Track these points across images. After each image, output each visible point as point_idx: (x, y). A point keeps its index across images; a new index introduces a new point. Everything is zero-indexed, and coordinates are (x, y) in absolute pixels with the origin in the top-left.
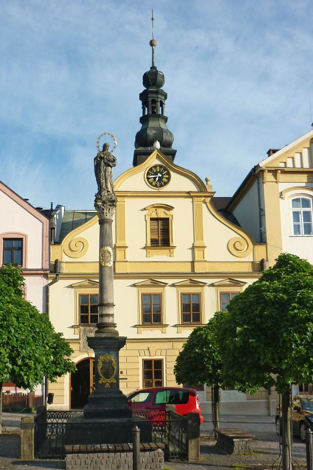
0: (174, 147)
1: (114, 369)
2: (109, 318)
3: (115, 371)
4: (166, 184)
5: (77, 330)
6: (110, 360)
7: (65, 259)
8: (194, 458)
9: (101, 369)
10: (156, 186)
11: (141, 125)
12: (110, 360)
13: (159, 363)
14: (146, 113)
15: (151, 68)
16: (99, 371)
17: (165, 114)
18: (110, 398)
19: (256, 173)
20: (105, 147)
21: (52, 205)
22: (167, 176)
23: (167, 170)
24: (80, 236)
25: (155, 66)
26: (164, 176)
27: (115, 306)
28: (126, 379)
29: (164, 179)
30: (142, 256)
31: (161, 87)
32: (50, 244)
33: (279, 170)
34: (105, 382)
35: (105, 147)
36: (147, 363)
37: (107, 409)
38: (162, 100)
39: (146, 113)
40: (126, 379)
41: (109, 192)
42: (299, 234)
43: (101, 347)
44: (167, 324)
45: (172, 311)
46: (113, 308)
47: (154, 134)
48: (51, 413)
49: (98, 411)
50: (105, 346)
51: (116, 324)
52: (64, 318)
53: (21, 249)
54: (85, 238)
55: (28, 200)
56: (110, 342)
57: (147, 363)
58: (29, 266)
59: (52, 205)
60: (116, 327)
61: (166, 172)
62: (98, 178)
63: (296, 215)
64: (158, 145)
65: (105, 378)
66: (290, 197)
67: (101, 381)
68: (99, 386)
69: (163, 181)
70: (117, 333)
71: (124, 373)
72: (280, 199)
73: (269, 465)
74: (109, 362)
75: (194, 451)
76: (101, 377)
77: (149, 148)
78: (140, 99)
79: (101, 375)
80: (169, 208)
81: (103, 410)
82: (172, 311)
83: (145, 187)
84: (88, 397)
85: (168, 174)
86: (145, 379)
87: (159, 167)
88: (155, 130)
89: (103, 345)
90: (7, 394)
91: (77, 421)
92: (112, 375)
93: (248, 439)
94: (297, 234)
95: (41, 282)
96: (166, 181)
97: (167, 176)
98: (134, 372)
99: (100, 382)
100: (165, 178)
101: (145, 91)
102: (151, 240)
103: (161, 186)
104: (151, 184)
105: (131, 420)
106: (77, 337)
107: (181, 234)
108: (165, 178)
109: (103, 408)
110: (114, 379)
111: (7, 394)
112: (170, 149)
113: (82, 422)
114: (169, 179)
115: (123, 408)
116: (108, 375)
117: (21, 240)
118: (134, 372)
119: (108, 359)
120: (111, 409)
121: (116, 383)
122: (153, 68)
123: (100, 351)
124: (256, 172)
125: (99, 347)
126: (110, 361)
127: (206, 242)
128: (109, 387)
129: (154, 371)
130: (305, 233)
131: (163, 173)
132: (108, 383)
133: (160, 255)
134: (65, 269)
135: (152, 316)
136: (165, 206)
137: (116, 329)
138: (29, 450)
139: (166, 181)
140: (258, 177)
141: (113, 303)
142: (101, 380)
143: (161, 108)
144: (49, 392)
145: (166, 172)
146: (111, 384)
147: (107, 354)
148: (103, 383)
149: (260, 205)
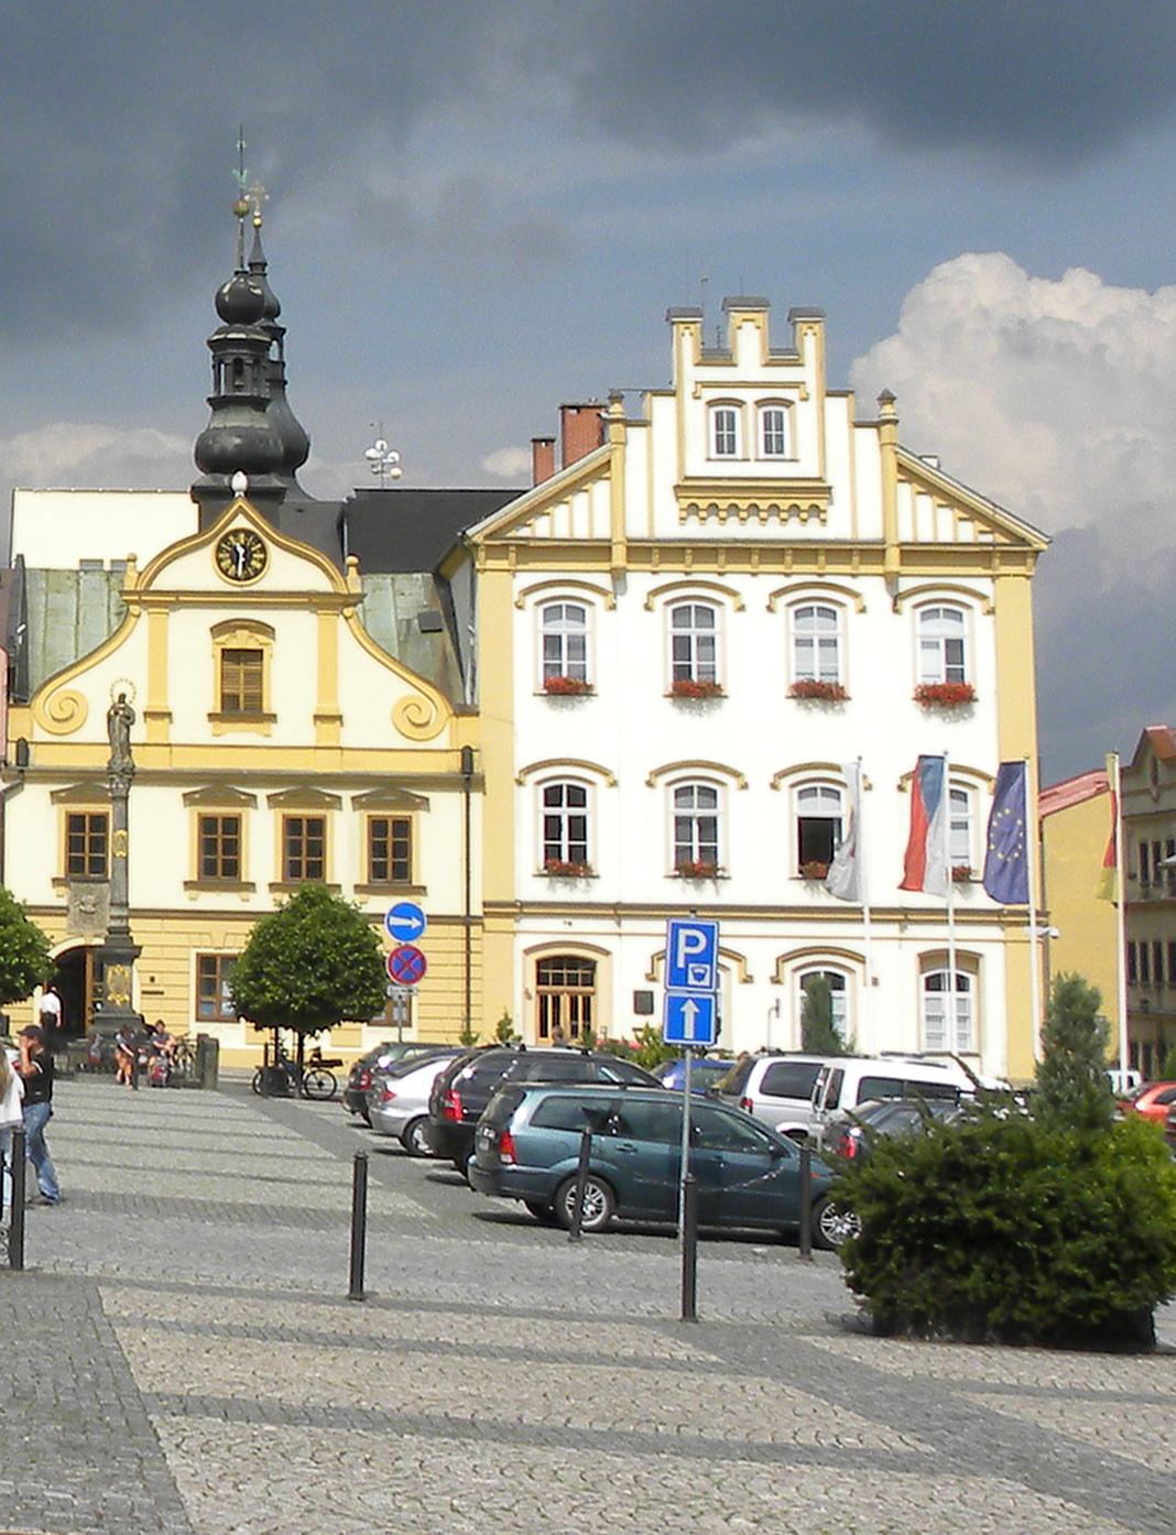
4: (257, 572)
5: (62, 890)
7: (40, 736)
10: (236, 578)
20: (122, 697)
22: (262, 556)
23: (260, 541)
24: (71, 686)
28: (162, 993)
29: (253, 563)
30: (204, 732)
32: (9, 706)
35: (122, 697)
40: (162, 993)
47: (237, 446)
48: (694, 912)
73: (1075, 1490)
80: (268, 630)
83: (212, 580)
84: (475, 1073)
85: (263, 550)
88: (239, 436)
96: (259, 566)
97: (262, 556)
98: (178, 979)
103: (248, 578)
104: (225, 572)
106: (63, 902)
114: (263, 562)
118: (178, 979)
134: (39, 758)
139: (259, 566)
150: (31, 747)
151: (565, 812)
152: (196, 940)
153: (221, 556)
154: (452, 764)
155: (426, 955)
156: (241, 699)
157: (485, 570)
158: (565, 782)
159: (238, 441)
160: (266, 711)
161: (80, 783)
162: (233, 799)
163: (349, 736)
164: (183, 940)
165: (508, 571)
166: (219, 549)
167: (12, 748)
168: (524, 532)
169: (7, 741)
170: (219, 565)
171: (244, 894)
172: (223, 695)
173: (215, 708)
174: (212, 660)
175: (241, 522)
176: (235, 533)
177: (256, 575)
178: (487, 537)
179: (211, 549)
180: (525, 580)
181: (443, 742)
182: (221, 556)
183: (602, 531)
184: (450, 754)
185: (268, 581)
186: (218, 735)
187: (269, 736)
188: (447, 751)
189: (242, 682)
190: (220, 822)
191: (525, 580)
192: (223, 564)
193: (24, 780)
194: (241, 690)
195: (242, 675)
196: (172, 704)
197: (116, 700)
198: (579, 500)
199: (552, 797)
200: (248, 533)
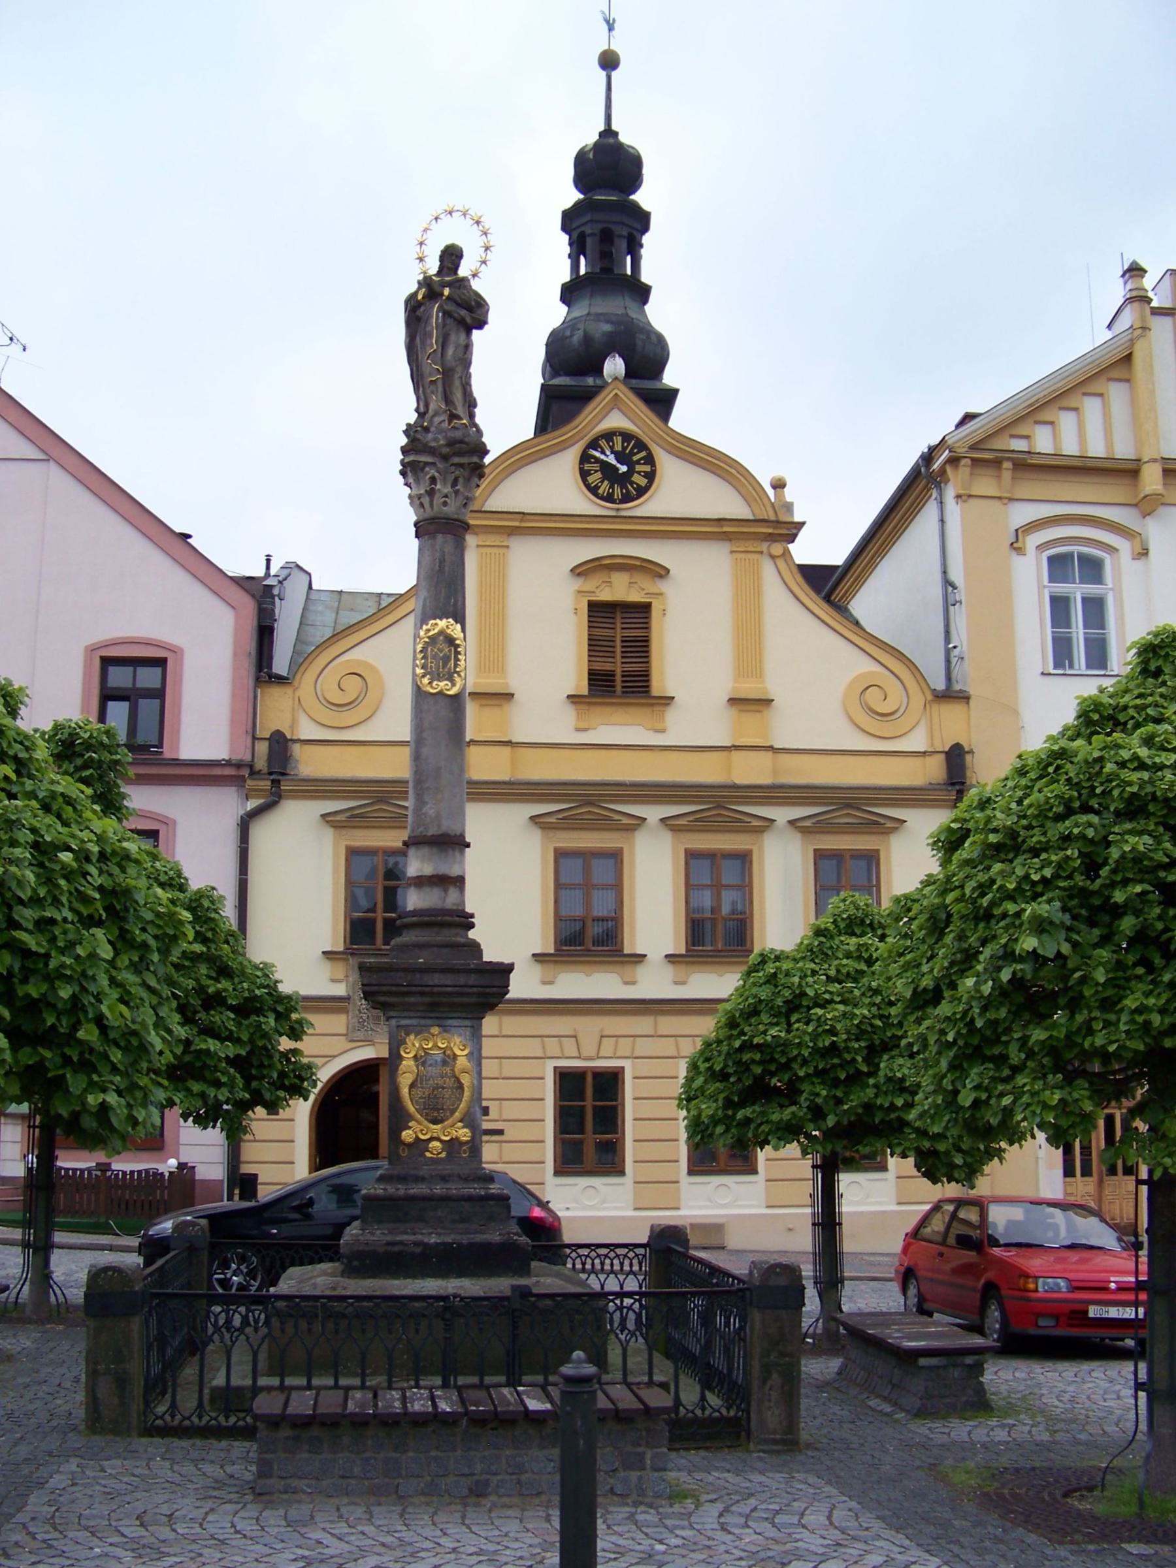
0: (670, 378)
1: (461, 1087)
2: (446, 891)
3: (467, 1094)
4: (642, 491)
6: (448, 1052)
7: (307, 730)
8: (778, 1436)
9: (412, 1086)
10: (609, 498)
11: (565, 309)
12: (448, 1052)
13: (609, 1083)
14: (582, 271)
15: (601, 134)
16: (405, 1091)
17: (645, 277)
18: (445, 1199)
19: (935, 466)
21: (268, 561)
22: (647, 468)
25: (614, 127)
26: (638, 468)
27: (468, 845)
28: (500, 1132)
31: (634, 192)
33: (1009, 459)
34: (427, 1137)
36: (570, 1083)
37: (433, 1240)
38: (635, 233)
39: (582, 271)
41: (459, 418)
42: (1071, 667)
43: (412, 999)
44: (639, 952)
45: (654, 909)
46: (462, 853)
47: (605, 334)
49: (396, 1249)
50: (427, 999)
51: (472, 916)
52: (295, 921)
53: (159, 694)
54: (370, 661)
55: (190, 536)
56: (449, 982)
57: (570, 1083)
58: (187, 752)
59: (268, 561)
60: (472, 926)
61: (644, 454)
62: (417, 366)
63: (1060, 606)
64: (614, 366)
65: (426, 1123)
66: (1041, 548)
67: (410, 1132)
68: (404, 1153)
69: (632, 483)
70: (475, 948)
71: (493, 1114)
72: (1014, 553)
74: (444, 1063)
75: (777, 1412)
76: (412, 1118)
77: (590, 381)
78: (565, 228)
79: (412, 1109)
80: (659, 572)
81: (416, 1244)
82: (654, 909)
85: (650, 460)
86: (562, 1133)
87: (620, 438)
88: (608, 322)
89: (422, 994)
90: (99, 1173)
91: (315, 1286)
92: (453, 1112)
93: (977, 1357)
94: (1064, 667)
95: (226, 806)
96: (643, 482)
97: (647, 468)
99: (407, 1135)
100: (639, 473)
101: (578, 205)
102: (589, 674)
103: (627, 498)
104: (593, 490)
105: (527, 1286)
106: (340, 990)
107: (691, 651)
108: (639, 473)
109: (419, 1237)
110: (460, 1124)
111: (99, 1173)
112: (657, 385)
113: (334, 1289)
114: (651, 476)
115: (495, 1237)
116: (438, 1110)
117: (161, 662)
119: (440, 1048)
120: (449, 1239)
121: (467, 1142)
122: (608, 133)
123: (410, 1018)
124: (936, 466)
125: (407, 999)
126: (449, 1056)
127: (773, 686)
128: (443, 1155)
129: (595, 1107)
130: (1088, 667)
131: (635, 458)
132: (438, 1139)
133: (619, 727)
134: (310, 763)
135: (588, 933)
136: (638, 563)
137: (472, 934)
138: (116, 1401)
139: (643, 482)
140: (940, 483)
141: (462, 836)
142: (410, 1128)
143: (629, 258)
144: (246, 1169)
145: (644, 454)
146: (452, 1145)
147: (435, 1030)
148: (417, 1138)
149: (945, 572)
150: (296, 749)
151: (1077, 591)
152: (552, 1046)
153: (587, 467)
154: (934, 770)
155: (915, 1172)
156: (618, 678)
157: (970, 496)
158: (1076, 549)
159: (607, 328)
160: (656, 691)
161: (366, 801)
162: (608, 824)
163: (786, 730)
164: (533, 1047)
165: (1000, 498)
166: (585, 458)
167: (262, 748)
168: (1020, 445)
169: (254, 738)
170: (584, 480)
171: (628, 969)
172: (591, 673)
173: (578, 687)
174: (572, 618)
175: (616, 421)
176: (609, 436)
177: (639, 496)
178: (973, 447)
179: (569, 459)
180: (1023, 514)
181: (917, 741)
182: (587, 467)
183: (1124, 450)
184: (928, 759)
185: (655, 505)
186: (585, 730)
187: (663, 731)
188: (924, 754)
189: (619, 650)
190: (589, 1078)
191: (1023, 514)
192: (590, 479)
193: (280, 797)
194: (617, 665)
195: (618, 643)
196: (514, 682)
197: (433, 266)
198: (1091, 407)
199: (1059, 566)
200: (627, 436)
